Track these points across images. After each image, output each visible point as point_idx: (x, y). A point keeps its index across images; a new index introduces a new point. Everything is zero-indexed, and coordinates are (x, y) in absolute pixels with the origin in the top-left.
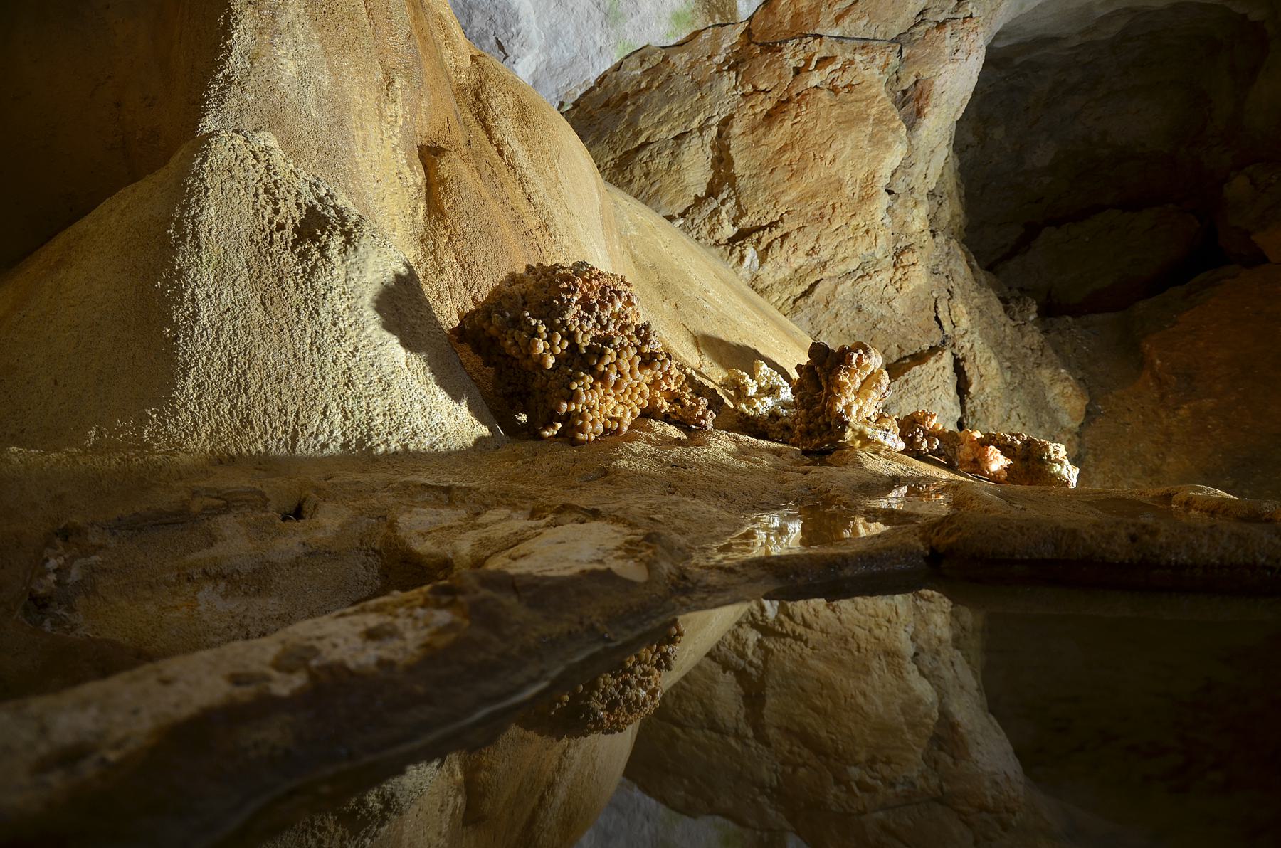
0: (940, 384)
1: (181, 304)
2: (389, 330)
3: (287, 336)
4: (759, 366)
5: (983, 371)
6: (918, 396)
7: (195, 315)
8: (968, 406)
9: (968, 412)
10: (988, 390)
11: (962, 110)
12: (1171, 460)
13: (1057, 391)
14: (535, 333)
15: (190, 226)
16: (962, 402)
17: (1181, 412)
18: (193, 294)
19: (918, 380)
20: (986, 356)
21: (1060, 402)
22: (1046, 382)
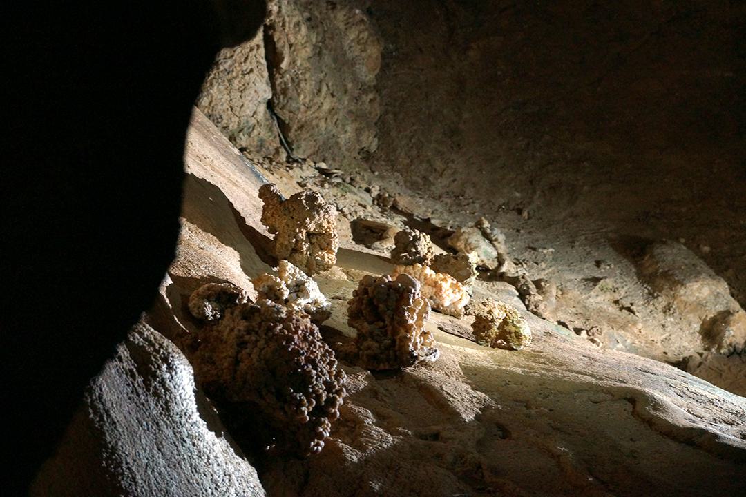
0: (254, 65)
1: (123, 474)
3: (180, 470)
5: (293, 40)
6: (230, 81)
7: (134, 478)
8: (279, 81)
9: (278, 89)
10: (299, 63)
12: (466, 115)
13: (352, 36)
14: (300, 403)
15: (101, 406)
16: (272, 78)
17: (472, 53)
18: (127, 463)
19: (229, 62)
20: (295, 20)
21: (356, 51)
22: (342, 26)
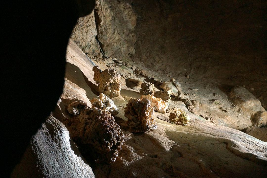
0: (91, 23)
1: (44, 170)
2: (72, 150)
3: (64, 168)
4: (143, 118)
5: (105, 14)
6: (82, 29)
7: (48, 171)
8: (100, 29)
9: (100, 32)
10: (107, 23)
11: (261, 141)
12: (167, 41)
13: (126, 13)
15: (36, 145)
16: (97, 28)
17: (169, 19)
18: (45, 166)
19: (82, 22)
20: (106, 7)
21: (127, 18)
22: (122, 9)
